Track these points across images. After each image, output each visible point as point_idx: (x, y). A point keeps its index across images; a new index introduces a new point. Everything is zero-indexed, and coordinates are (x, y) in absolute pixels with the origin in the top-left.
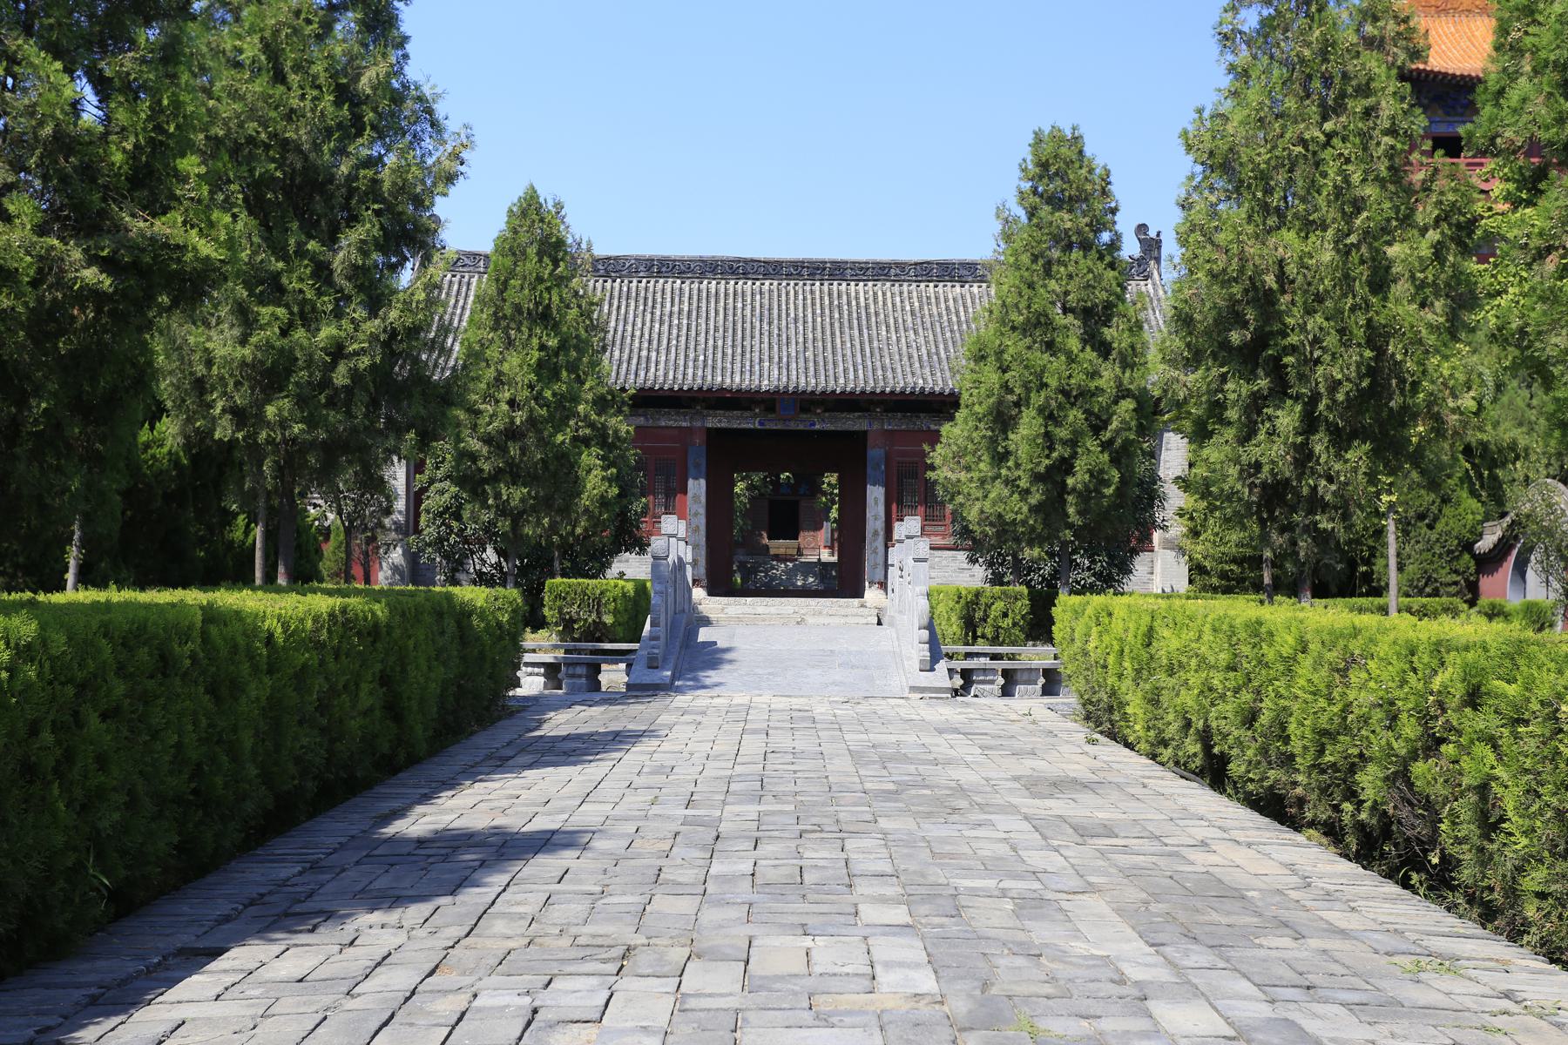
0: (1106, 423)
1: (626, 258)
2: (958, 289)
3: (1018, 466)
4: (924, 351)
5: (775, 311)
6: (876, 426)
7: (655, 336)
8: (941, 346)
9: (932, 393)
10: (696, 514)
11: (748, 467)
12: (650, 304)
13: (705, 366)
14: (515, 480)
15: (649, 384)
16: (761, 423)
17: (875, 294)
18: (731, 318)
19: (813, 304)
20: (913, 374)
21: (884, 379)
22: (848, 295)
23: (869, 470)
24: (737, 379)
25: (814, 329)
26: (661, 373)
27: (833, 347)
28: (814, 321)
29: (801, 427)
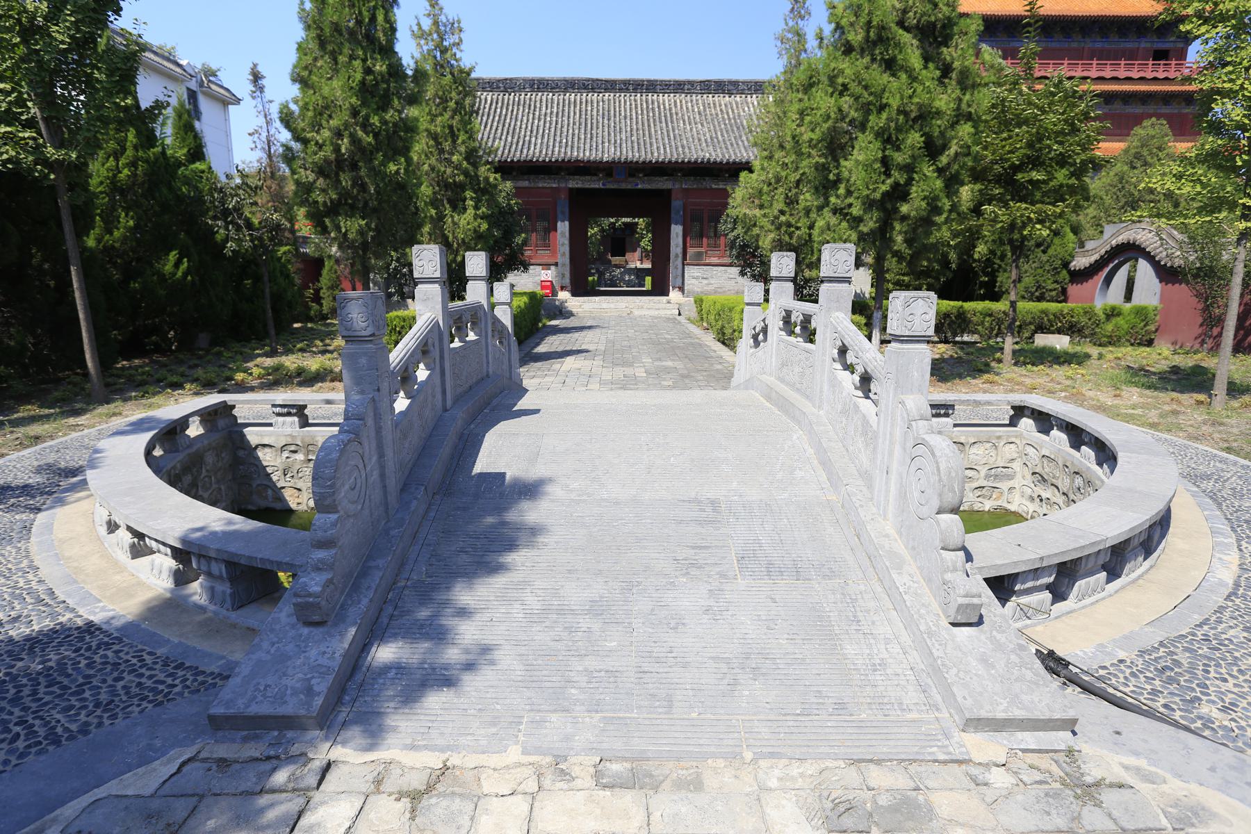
0: (945, 147)
1: (517, 79)
3: (849, 193)
9: (715, 162)
14: (352, 211)
26: (537, 151)
29: (629, 187)
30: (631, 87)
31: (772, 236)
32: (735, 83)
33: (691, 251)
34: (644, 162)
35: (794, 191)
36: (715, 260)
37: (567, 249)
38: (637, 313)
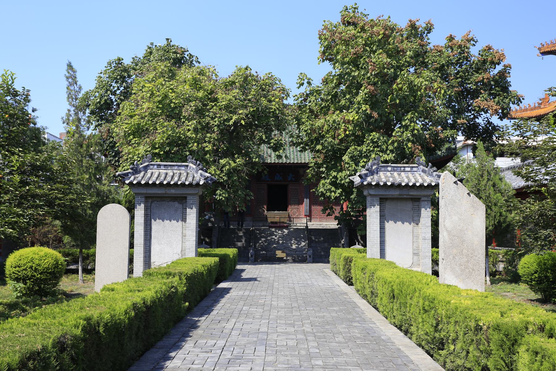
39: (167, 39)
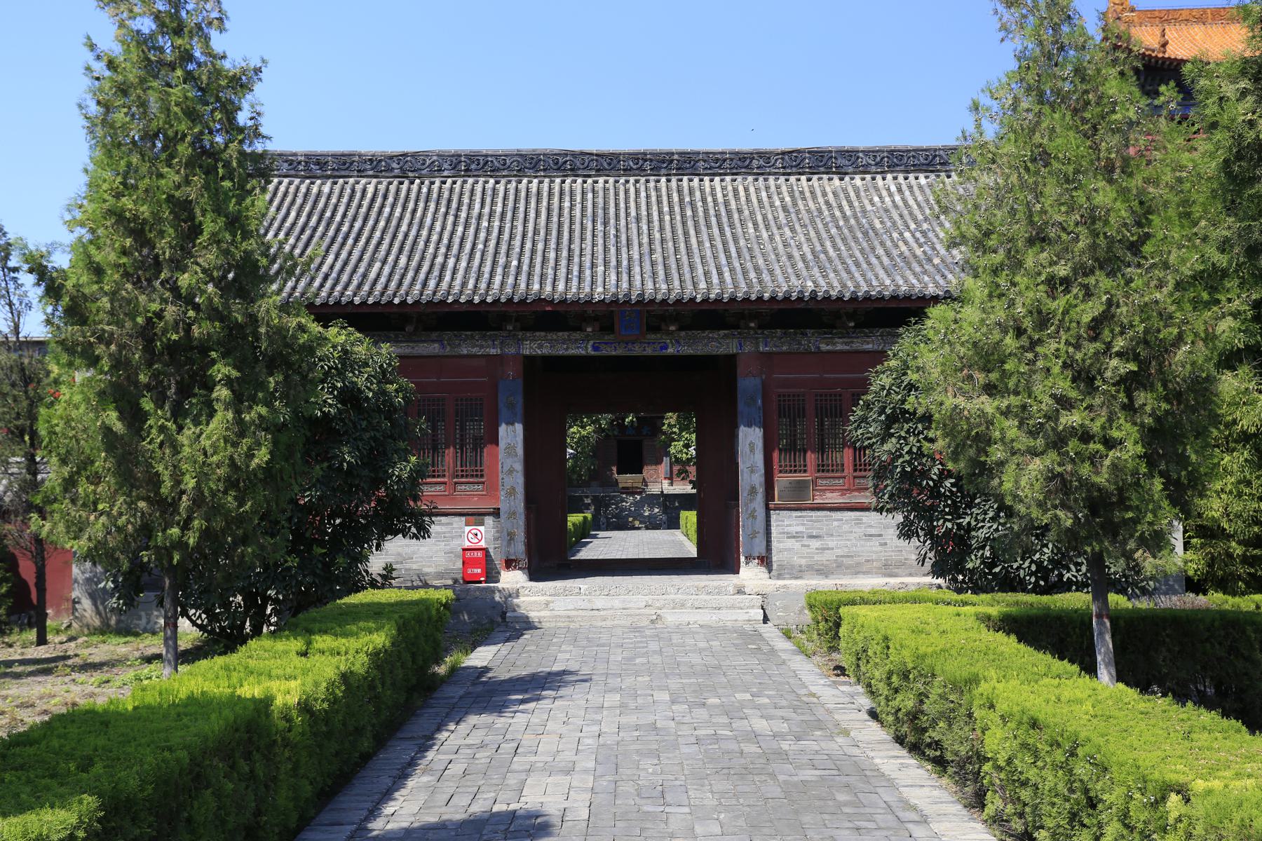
1: (427, 154)
2: (836, 181)
4: (806, 248)
5: (612, 210)
6: (748, 348)
7: (457, 240)
8: (828, 244)
9: (827, 299)
10: (511, 471)
11: (585, 407)
12: (452, 206)
13: (518, 273)
15: (439, 296)
16: (595, 348)
17: (735, 191)
18: (555, 219)
19: (659, 202)
20: (798, 276)
21: (760, 282)
22: (702, 191)
23: (741, 406)
24: (561, 287)
25: (662, 229)
26: (458, 282)
27: (688, 248)
28: (661, 220)
29: (649, 351)
30: (647, 166)
31: (1036, 465)
32: (850, 154)
33: (782, 481)
34: (678, 302)
35: (1091, 348)
36: (833, 498)
37: (519, 480)
38: (671, 618)
39: (263, 61)
